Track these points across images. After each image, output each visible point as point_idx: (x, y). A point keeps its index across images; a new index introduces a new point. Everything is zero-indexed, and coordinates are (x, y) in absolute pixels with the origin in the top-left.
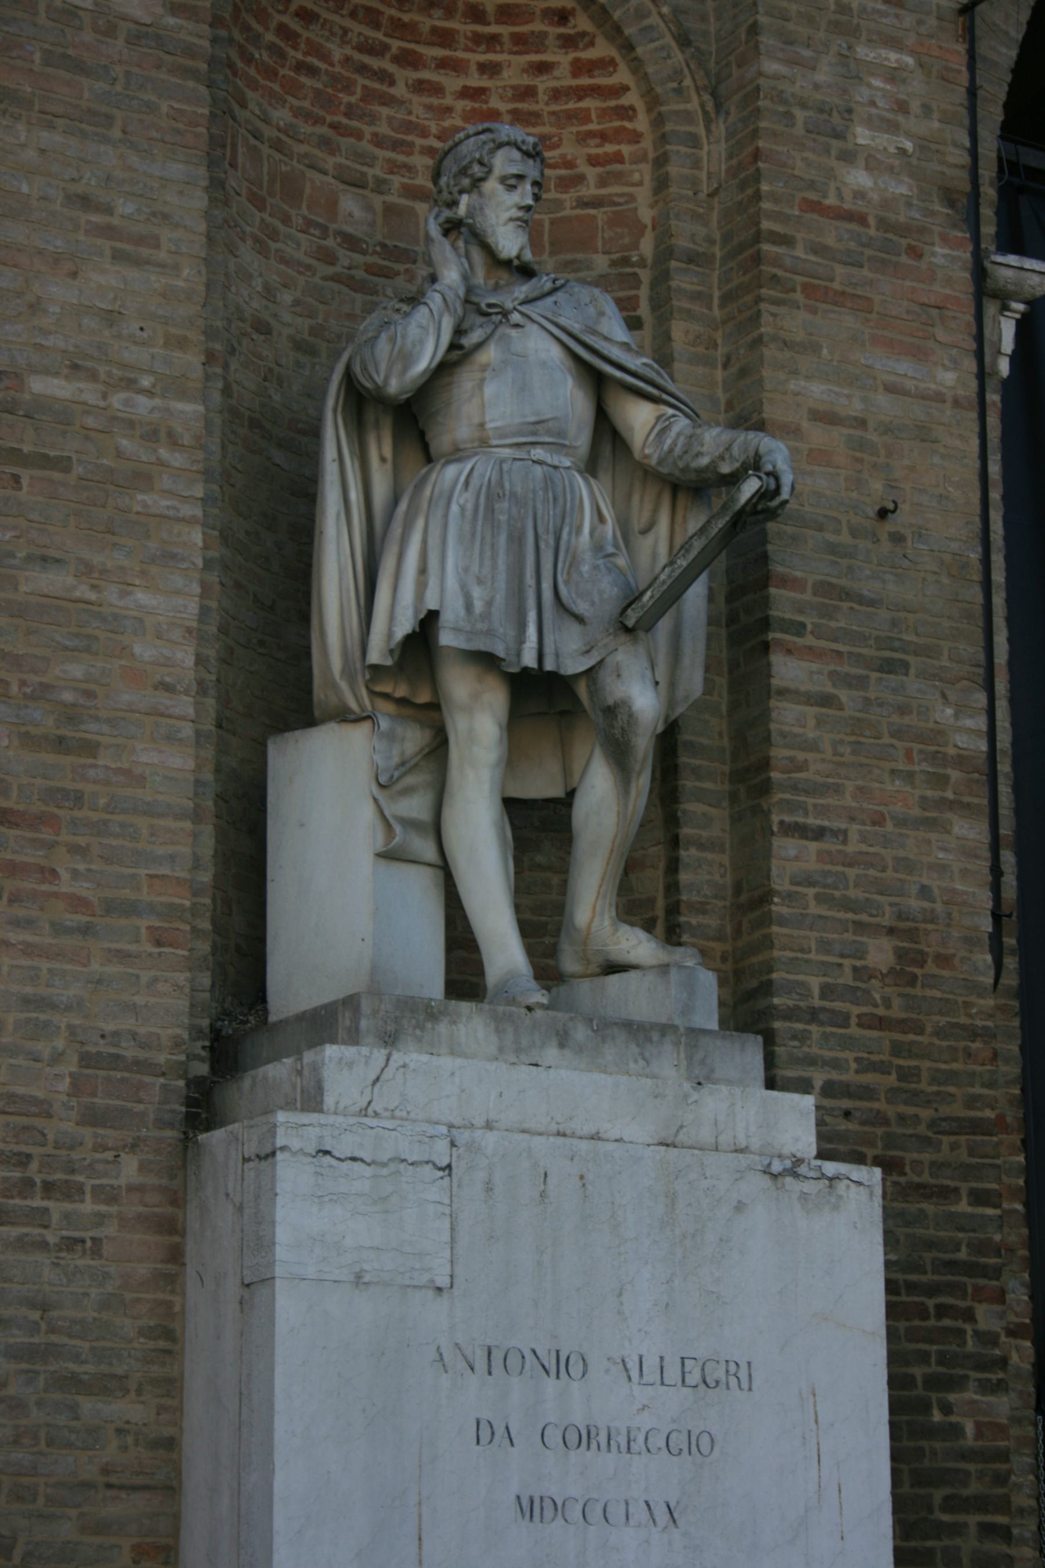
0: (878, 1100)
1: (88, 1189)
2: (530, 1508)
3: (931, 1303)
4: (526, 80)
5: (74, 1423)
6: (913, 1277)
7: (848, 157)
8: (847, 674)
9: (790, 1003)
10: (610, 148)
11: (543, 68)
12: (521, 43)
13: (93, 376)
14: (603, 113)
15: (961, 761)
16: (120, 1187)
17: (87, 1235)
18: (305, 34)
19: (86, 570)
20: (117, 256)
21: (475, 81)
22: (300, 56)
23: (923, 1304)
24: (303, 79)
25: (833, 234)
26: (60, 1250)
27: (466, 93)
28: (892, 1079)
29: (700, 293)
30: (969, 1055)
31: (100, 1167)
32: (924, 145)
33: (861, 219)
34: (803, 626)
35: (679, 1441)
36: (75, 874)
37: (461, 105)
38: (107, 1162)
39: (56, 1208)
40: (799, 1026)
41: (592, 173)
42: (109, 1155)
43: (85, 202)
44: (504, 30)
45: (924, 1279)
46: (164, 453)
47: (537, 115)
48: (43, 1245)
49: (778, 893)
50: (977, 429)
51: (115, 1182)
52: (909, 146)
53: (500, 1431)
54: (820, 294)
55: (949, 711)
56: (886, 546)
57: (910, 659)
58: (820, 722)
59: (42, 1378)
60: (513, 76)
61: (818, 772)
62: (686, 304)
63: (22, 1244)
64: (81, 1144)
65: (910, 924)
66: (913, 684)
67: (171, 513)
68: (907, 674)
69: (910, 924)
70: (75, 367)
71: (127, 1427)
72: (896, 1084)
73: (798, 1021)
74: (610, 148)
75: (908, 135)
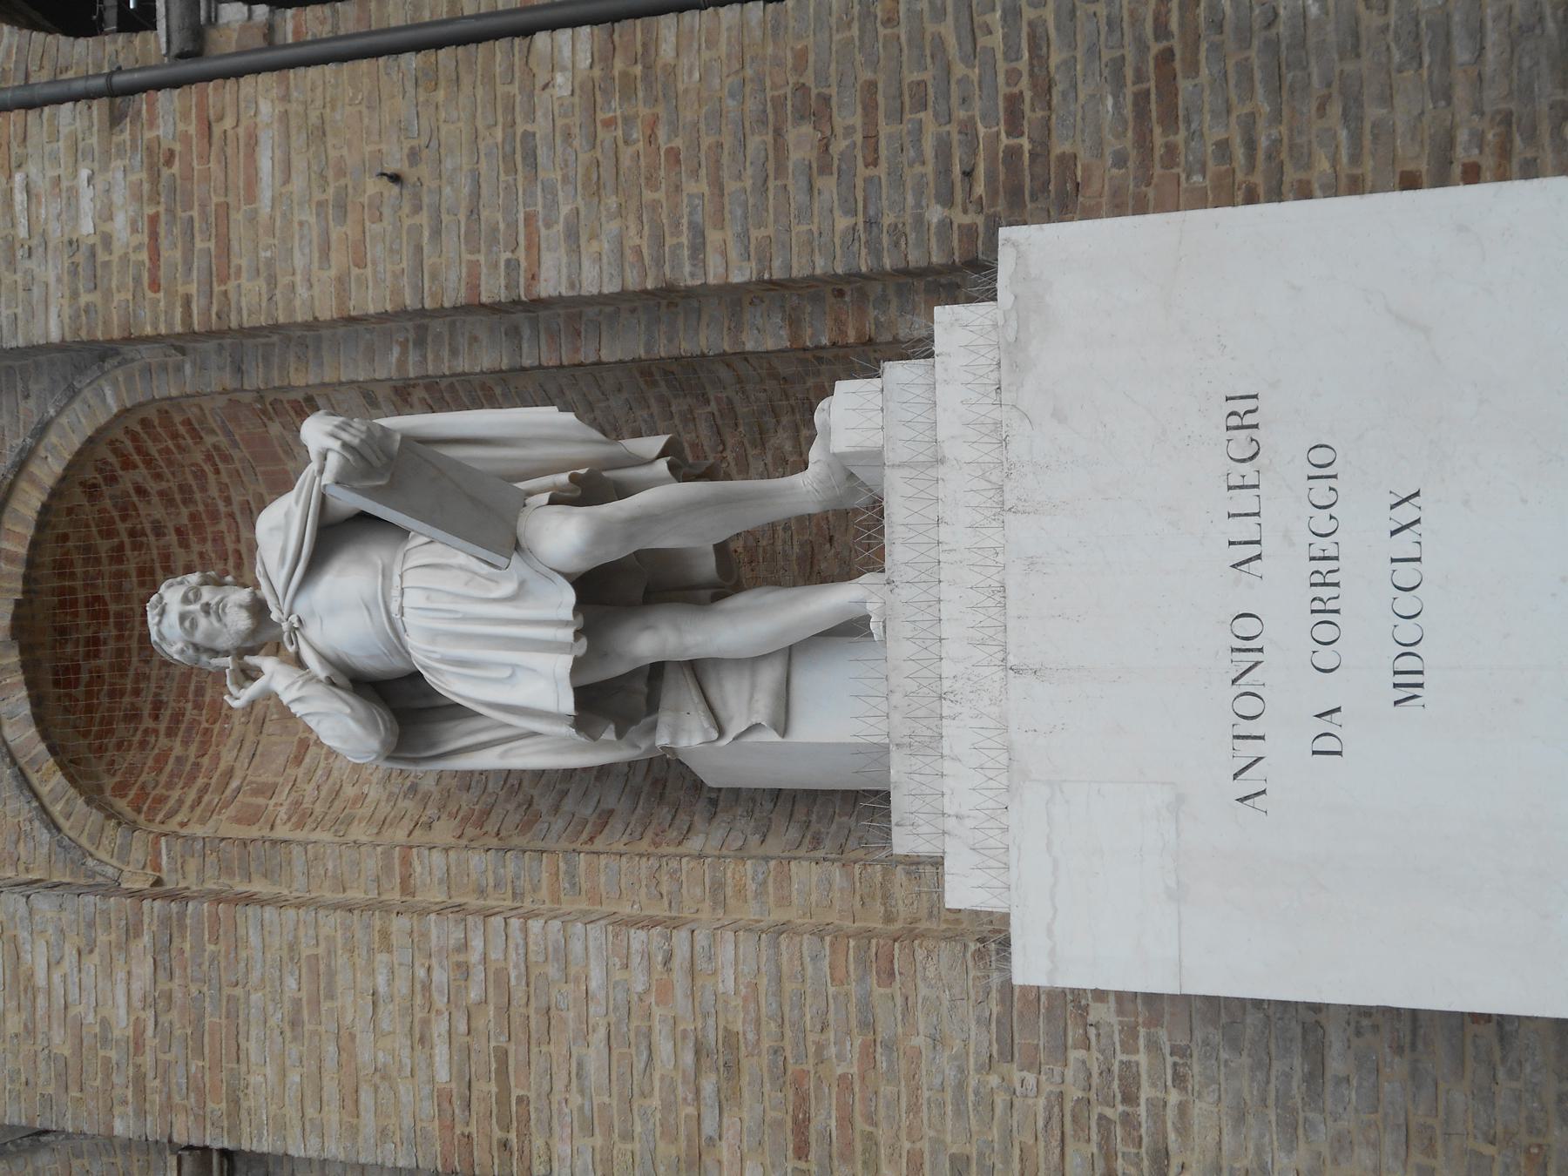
0: (949, 133)
1: (1125, 1058)
2: (1408, 687)
3: (1155, 48)
4: (155, 499)
5: (1354, 1083)
6: (1129, 73)
7: (107, 240)
8: (544, 207)
9: (864, 251)
10: (182, 430)
11: (141, 491)
12: (126, 511)
13: (426, 1022)
14: (156, 439)
15: (604, 57)
16: (1121, 1023)
17: (1170, 1060)
18: (172, 704)
19: (585, 1035)
20: (331, 996)
21: (172, 538)
22: (189, 706)
23: (1156, 58)
24: (207, 699)
25: (171, 254)
26: (1185, 1089)
27: (184, 544)
28: (926, 116)
29: (264, 358)
30: (889, 20)
31: (1103, 1041)
32: (77, 153)
33: (154, 220)
34: (508, 262)
35: (1321, 492)
36: (840, 1057)
37: (196, 548)
38: (1098, 1035)
39: (1146, 1092)
40: (885, 239)
41: (209, 440)
42: (1092, 1032)
43: (295, 1023)
44: (122, 527)
45: (1130, 58)
46: (474, 957)
47: (181, 487)
48: (1182, 1109)
49: (760, 272)
50: (302, 69)
51: (1117, 1028)
52: (84, 173)
53: (1323, 725)
54: (221, 268)
55: (560, 78)
56: (424, 170)
57: (519, 131)
58: (594, 236)
59: (1311, 1115)
60: (158, 512)
61: (640, 233)
62: (275, 373)
63: (1183, 1129)
64: (1084, 1062)
65: (769, 109)
66: (541, 127)
67: (522, 951)
68: (534, 134)
69: (769, 109)
70: (422, 1040)
71: (1353, 1024)
72: (930, 111)
73: (880, 243)
74: (182, 430)
75: (75, 175)
